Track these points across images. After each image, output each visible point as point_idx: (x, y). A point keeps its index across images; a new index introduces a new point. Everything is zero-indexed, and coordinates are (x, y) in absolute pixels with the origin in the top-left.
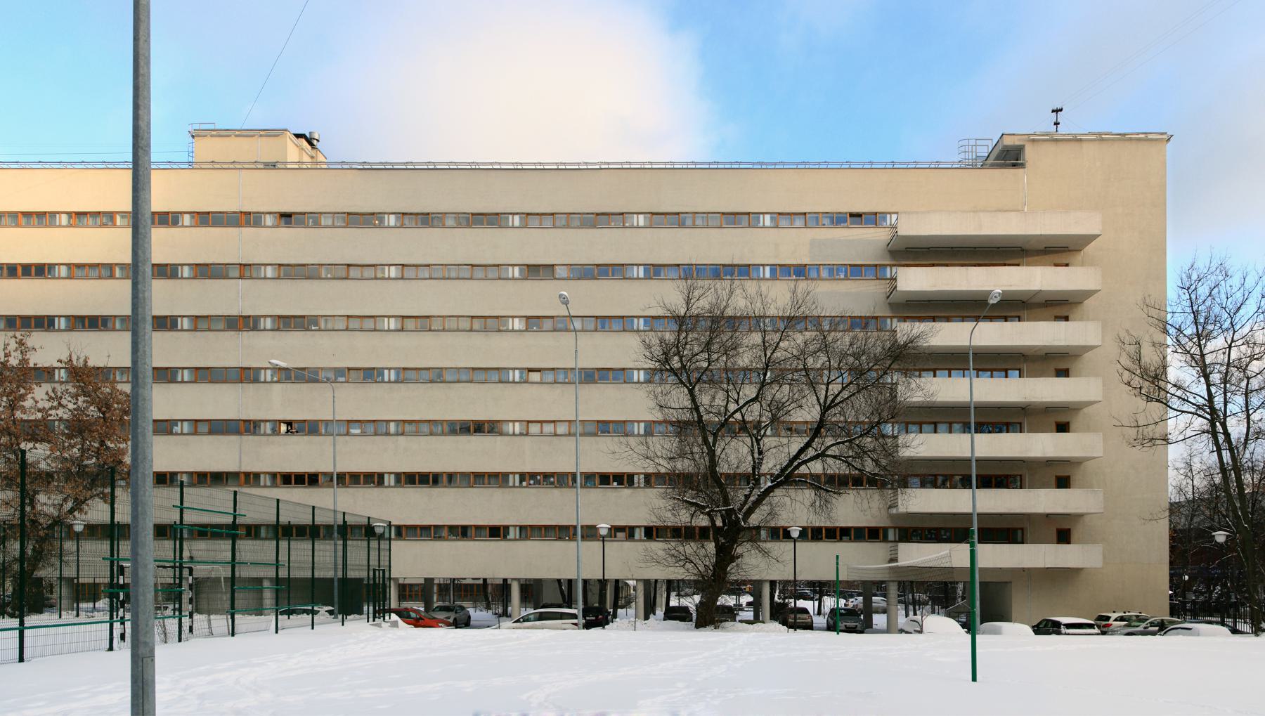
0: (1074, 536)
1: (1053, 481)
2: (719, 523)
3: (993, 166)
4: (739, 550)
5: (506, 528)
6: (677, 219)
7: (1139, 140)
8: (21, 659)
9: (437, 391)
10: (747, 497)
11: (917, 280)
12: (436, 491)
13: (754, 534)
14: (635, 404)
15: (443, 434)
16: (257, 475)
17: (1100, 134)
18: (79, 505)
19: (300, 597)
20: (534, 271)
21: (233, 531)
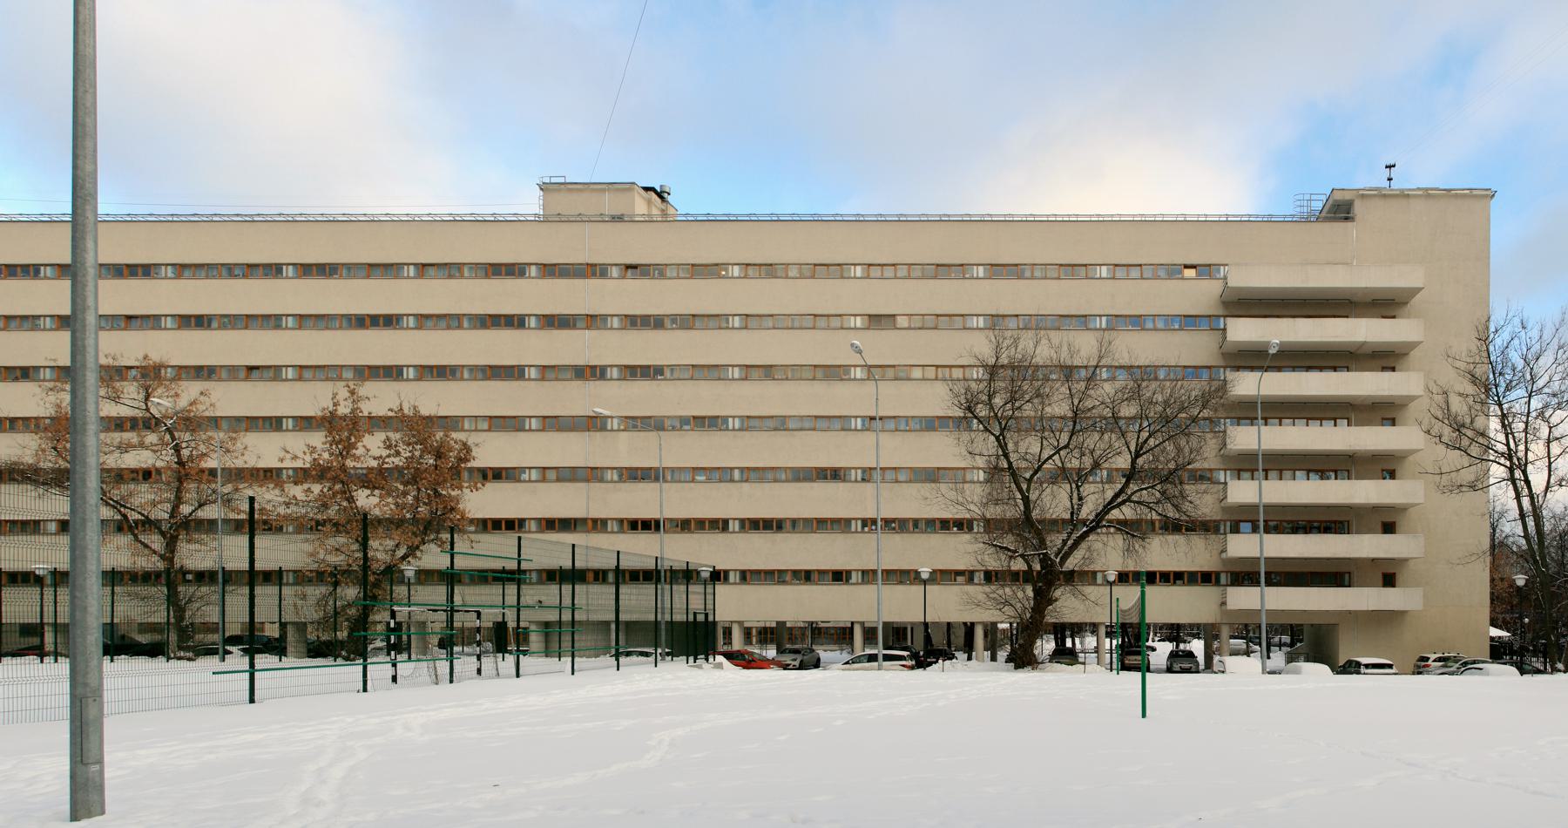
0: (1399, 579)
1: (1379, 527)
2: (1038, 567)
3: (1327, 219)
4: (1057, 593)
5: (849, 572)
6: (1013, 271)
7: (1465, 196)
8: (252, 700)
9: (780, 438)
10: (1064, 542)
11: (1244, 331)
12: (779, 536)
13: (1071, 577)
15: (787, 481)
16: (604, 522)
17: (1427, 189)
18: (412, 551)
19: (631, 639)
20: (878, 321)
21: (512, 577)
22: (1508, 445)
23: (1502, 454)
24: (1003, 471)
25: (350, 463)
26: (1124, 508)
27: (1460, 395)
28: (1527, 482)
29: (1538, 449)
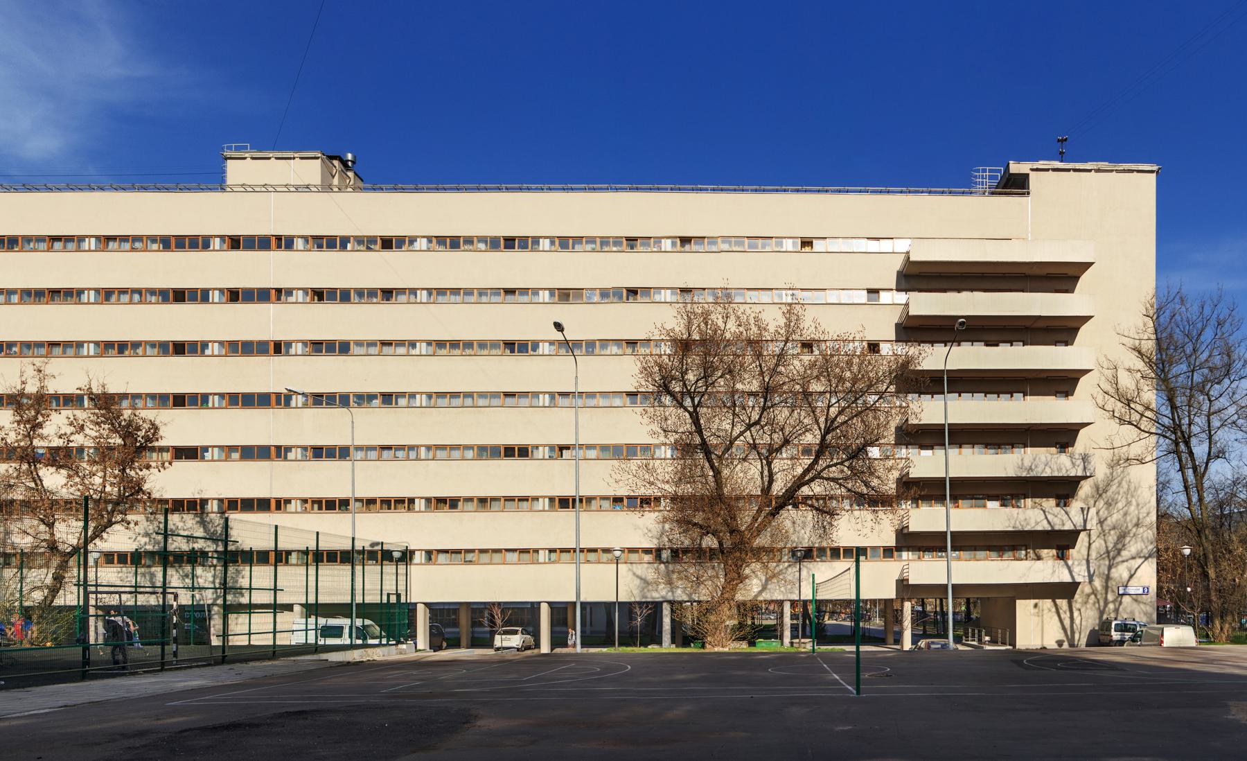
13: (758, 553)
14: (635, 426)
22: (1173, 420)
23: (1168, 428)
24: (696, 448)
25: (36, 442)
26: (812, 484)
27: (1129, 370)
28: (1191, 453)
29: (1200, 421)
